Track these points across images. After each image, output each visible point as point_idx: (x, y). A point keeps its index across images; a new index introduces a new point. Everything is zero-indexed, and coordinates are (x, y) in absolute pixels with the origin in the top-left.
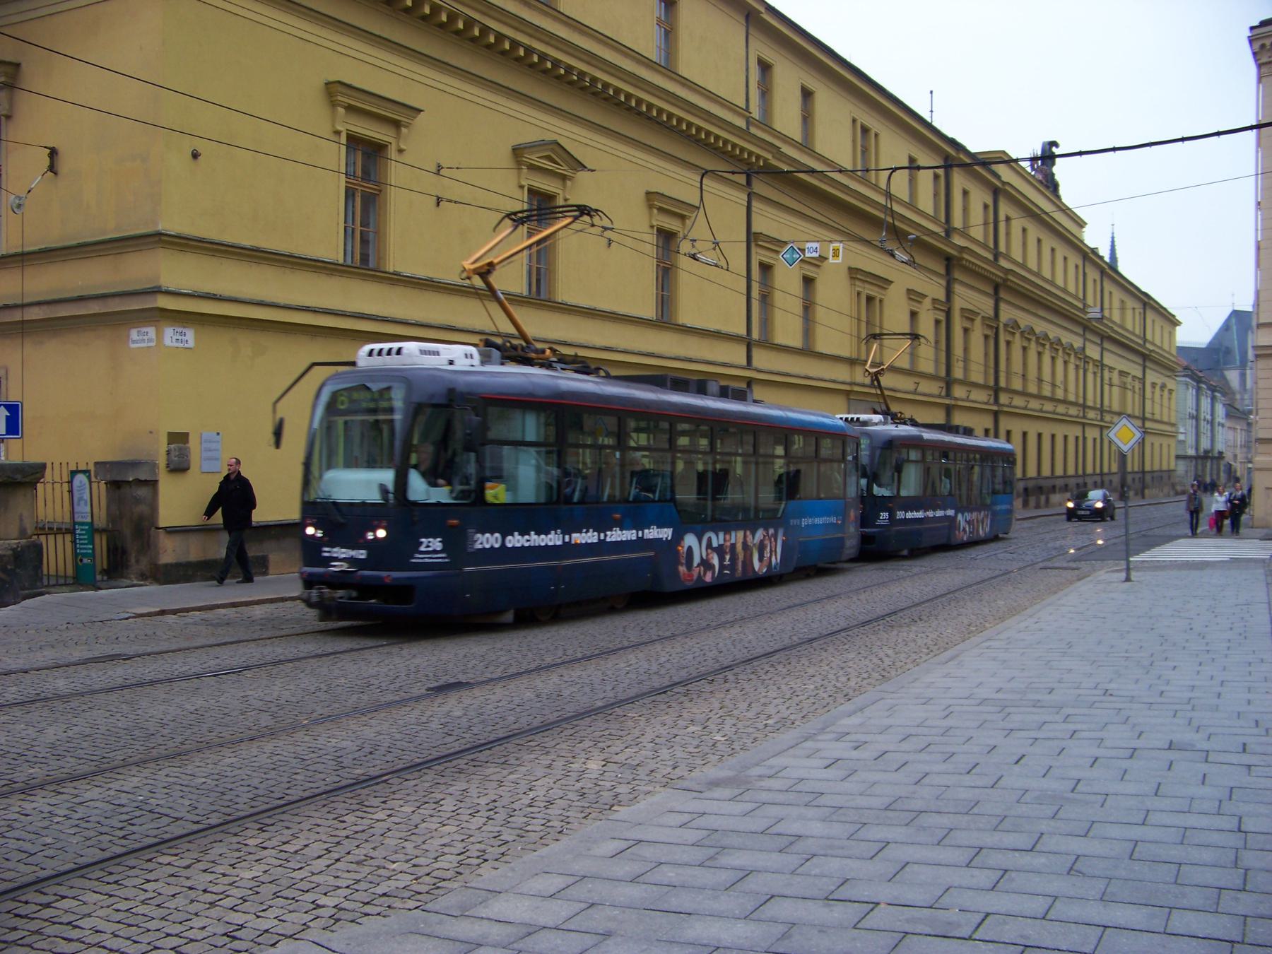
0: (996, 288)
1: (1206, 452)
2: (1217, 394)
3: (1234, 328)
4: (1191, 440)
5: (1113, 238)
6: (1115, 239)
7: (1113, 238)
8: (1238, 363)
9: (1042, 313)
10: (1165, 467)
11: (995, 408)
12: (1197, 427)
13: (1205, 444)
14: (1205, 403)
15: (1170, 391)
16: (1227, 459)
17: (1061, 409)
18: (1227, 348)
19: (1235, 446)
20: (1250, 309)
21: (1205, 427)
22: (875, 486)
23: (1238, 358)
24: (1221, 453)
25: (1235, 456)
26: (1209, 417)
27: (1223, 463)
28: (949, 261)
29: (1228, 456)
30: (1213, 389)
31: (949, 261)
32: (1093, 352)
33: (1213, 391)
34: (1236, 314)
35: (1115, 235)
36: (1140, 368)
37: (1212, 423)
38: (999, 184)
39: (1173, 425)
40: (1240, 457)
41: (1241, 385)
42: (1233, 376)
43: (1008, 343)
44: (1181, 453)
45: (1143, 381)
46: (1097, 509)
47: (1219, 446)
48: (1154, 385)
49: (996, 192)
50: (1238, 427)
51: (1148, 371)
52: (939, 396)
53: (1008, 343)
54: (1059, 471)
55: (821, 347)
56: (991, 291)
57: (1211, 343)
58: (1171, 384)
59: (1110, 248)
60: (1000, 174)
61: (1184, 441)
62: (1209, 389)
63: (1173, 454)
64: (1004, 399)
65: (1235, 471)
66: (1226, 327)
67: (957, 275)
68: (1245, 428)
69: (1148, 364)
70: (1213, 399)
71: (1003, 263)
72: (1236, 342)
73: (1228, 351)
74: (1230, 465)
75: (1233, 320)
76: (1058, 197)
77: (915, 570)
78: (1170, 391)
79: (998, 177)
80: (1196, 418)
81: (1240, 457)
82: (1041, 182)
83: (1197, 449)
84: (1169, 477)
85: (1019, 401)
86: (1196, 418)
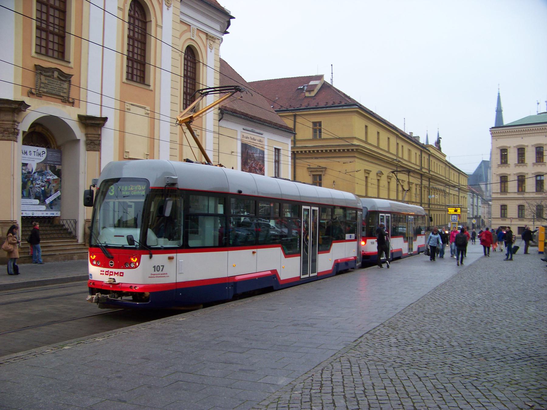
0: (429, 179)
1: (476, 216)
2: (479, 196)
3: (483, 167)
4: (471, 213)
5: (438, 133)
6: (439, 134)
7: (438, 133)
8: (485, 180)
9: (438, 183)
10: (464, 222)
11: (429, 209)
12: (473, 209)
13: (475, 214)
14: (475, 199)
15: (466, 198)
16: (482, 218)
17: (436, 207)
18: (481, 175)
19: (484, 213)
20: (489, 160)
21: (475, 207)
22: (249, 240)
23: (484, 178)
24: (480, 216)
25: (484, 217)
26: (476, 204)
27: (481, 219)
28: (422, 175)
29: (482, 217)
30: (477, 195)
31: (422, 175)
32: (447, 191)
33: (477, 195)
34: (484, 162)
35: (439, 132)
36: (458, 192)
37: (477, 206)
38: (430, 153)
39: (466, 208)
40: (486, 217)
41: (485, 188)
42: (483, 187)
43: (424, 191)
44: (469, 217)
45: (459, 196)
46: (446, 234)
47: (480, 214)
48: (461, 197)
49: (429, 155)
50: (485, 207)
51: (460, 193)
52: (427, 208)
53: (431, 192)
54: (438, 225)
55: (391, 198)
56: (428, 180)
57: (475, 171)
58: (466, 196)
59: (437, 136)
60: (430, 150)
61: (469, 213)
62: (477, 195)
63: (466, 218)
64: (431, 206)
65: (485, 222)
66: (480, 167)
67: (423, 178)
68: (488, 207)
69: (460, 191)
70: (478, 198)
71: (431, 173)
72: (484, 173)
73: (481, 176)
74: (483, 220)
75: (483, 164)
76: (441, 151)
77: (248, 301)
78: (466, 198)
79: (429, 151)
80: (472, 205)
81: (486, 217)
82: (437, 149)
83: (473, 215)
84: (466, 224)
85: (433, 207)
86: (472, 205)
